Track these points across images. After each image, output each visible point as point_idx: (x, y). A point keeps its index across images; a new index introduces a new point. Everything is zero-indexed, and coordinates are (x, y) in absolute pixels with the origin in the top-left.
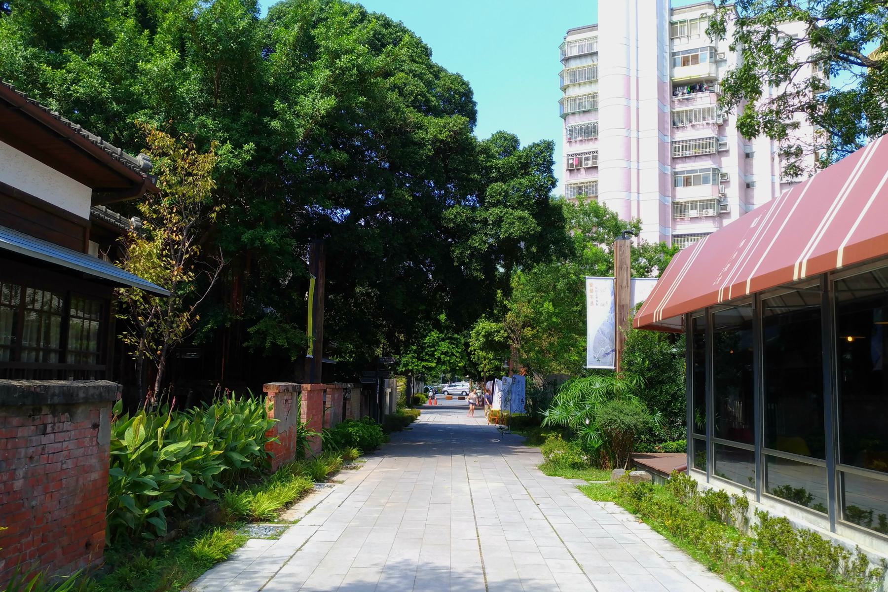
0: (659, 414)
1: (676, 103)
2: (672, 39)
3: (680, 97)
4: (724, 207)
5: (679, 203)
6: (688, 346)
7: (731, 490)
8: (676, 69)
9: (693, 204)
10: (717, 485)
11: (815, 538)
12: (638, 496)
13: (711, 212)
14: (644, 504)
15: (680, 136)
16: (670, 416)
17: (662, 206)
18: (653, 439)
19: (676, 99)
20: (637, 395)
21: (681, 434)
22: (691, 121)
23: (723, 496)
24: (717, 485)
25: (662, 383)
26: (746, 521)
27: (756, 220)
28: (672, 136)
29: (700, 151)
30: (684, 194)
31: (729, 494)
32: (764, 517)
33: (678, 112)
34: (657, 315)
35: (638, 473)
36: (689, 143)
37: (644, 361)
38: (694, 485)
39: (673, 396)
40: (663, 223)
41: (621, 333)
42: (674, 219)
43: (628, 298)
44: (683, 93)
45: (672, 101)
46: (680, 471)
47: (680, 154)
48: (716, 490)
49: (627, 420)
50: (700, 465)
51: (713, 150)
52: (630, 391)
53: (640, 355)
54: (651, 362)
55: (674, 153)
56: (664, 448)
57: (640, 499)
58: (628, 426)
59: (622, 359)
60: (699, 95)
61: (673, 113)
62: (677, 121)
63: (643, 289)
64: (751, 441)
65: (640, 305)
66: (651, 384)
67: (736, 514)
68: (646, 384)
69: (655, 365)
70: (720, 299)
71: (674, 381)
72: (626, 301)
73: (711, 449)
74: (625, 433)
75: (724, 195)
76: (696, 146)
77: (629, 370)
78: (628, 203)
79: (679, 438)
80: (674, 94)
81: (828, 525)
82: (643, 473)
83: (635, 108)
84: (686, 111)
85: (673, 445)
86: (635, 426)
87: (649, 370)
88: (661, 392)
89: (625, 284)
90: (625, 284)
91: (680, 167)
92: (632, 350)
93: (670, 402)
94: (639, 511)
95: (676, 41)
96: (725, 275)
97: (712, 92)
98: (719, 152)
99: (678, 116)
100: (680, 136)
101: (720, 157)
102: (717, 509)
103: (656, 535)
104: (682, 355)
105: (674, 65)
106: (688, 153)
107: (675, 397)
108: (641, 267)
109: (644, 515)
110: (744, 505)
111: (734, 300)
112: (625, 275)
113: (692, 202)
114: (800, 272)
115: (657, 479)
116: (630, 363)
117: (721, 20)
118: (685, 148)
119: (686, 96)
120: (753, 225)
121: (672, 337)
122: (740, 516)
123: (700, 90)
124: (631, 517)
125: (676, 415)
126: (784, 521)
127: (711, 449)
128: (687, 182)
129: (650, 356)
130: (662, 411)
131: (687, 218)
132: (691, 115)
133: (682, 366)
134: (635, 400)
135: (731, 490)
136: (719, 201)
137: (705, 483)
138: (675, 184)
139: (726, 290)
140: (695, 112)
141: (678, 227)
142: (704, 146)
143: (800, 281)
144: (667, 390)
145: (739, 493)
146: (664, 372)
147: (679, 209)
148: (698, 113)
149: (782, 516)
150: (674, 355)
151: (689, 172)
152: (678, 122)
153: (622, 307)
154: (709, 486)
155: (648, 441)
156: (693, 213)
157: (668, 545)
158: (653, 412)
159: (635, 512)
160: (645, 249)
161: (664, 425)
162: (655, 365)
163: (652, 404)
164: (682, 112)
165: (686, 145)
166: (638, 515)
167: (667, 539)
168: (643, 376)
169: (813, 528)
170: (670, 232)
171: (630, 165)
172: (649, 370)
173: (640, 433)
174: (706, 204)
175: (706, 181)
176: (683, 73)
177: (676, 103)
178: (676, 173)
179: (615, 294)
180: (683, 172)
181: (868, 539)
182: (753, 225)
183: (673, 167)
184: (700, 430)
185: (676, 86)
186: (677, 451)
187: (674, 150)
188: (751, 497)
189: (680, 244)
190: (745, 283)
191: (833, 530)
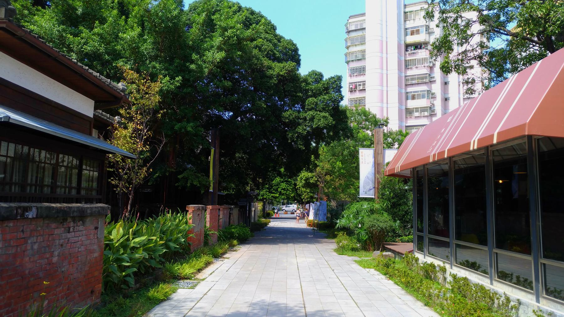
0: (398, 222)
2: (405, 21)
3: (410, 52)
4: (433, 111)
5: (409, 109)
6: (414, 186)
7: (437, 262)
9: (417, 109)
10: (429, 260)
12: (387, 266)
13: (426, 114)
15: (409, 73)
16: (404, 227)
17: (400, 110)
18: (395, 235)
19: (407, 53)
21: (410, 232)
22: (415, 65)
23: (432, 266)
25: (400, 205)
26: (445, 279)
27: (450, 118)
29: (420, 81)
30: (412, 104)
31: (436, 265)
32: (454, 277)
33: (408, 60)
35: (387, 253)
38: (417, 260)
39: (406, 212)
40: (400, 119)
41: (378, 179)
42: (406, 118)
45: (405, 54)
46: (409, 252)
47: (410, 82)
48: (429, 262)
49: (381, 225)
50: (421, 249)
51: (427, 80)
54: (394, 194)
56: (401, 240)
57: (388, 267)
58: (382, 228)
60: (419, 51)
62: (407, 65)
63: (390, 155)
64: (447, 236)
65: (388, 164)
66: (394, 205)
67: (440, 275)
68: (391, 206)
70: (431, 160)
71: (406, 204)
72: (380, 161)
73: (426, 241)
75: (433, 104)
76: (418, 78)
77: (382, 198)
80: (406, 50)
82: (390, 253)
87: (393, 198)
88: (400, 210)
89: (380, 152)
90: (380, 152)
91: (410, 89)
92: (384, 187)
93: (404, 215)
94: (387, 274)
95: (408, 22)
96: (434, 147)
97: (427, 49)
98: (430, 82)
100: (409, 73)
102: (429, 273)
103: (397, 287)
104: (410, 190)
105: (406, 35)
106: (413, 82)
107: (407, 213)
109: (390, 276)
110: (444, 270)
111: (438, 161)
112: (380, 147)
113: (416, 108)
114: (474, 146)
115: (397, 256)
116: (383, 195)
118: (412, 79)
120: (449, 121)
121: (406, 180)
122: (442, 276)
123: (420, 48)
124: (383, 277)
126: (465, 279)
127: (426, 241)
128: (413, 98)
129: (393, 190)
130: (400, 220)
133: (411, 196)
134: (385, 214)
135: (437, 262)
136: (430, 108)
137: (423, 259)
138: (407, 99)
139: (434, 155)
142: (422, 78)
143: (474, 150)
145: (441, 264)
146: (401, 199)
147: (409, 112)
148: (419, 60)
150: (406, 190)
153: (378, 164)
154: (425, 260)
155: (393, 236)
156: (417, 114)
157: (403, 292)
158: (395, 221)
159: (385, 274)
161: (401, 228)
162: (396, 196)
164: (411, 60)
165: (413, 77)
166: (387, 276)
168: (390, 201)
169: (481, 282)
172: (393, 198)
173: (388, 232)
174: (423, 109)
175: (423, 97)
176: (411, 39)
178: (407, 93)
180: (411, 92)
181: (523, 294)
182: (449, 121)
183: (406, 90)
185: (407, 46)
186: (408, 242)
187: (406, 80)
188: (447, 266)
189: (410, 131)
191: (492, 284)
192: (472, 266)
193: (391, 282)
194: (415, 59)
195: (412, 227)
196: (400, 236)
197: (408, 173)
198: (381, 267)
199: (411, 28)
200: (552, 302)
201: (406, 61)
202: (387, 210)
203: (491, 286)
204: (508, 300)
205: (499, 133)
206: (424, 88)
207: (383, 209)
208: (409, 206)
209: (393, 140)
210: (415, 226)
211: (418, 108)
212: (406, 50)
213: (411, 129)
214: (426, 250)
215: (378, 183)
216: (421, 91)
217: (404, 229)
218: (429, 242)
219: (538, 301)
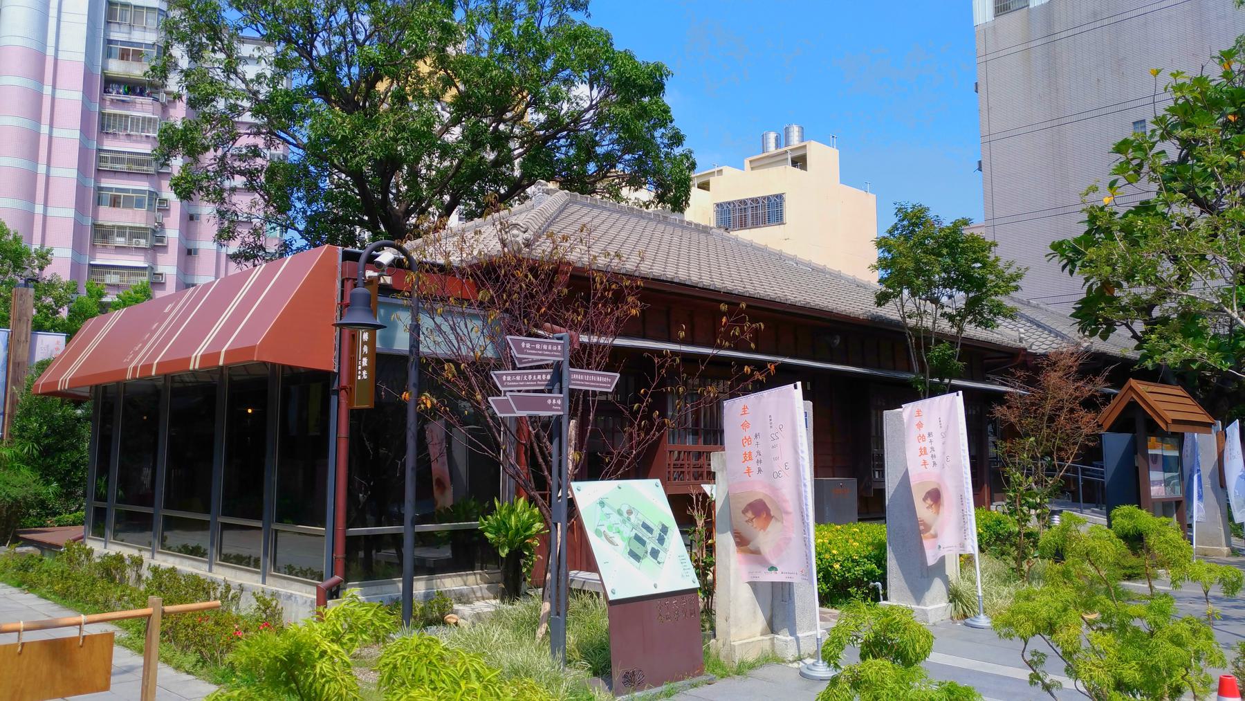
0: (55, 484)
1: (108, 103)
2: (108, 23)
3: (114, 96)
4: (161, 239)
5: (102, 226)
6: (95, 408)
7: (127, 552)
8: (111, 61)
9: (121, 231)
10: (113, 549)
11: (195, 577)
12: (25, 568)
13: (143, 243)
14: (32, 574)
15: (110, 145)
16: (67, 495)
17: (78, 227)
18: (46, 511)
19: (108, 97)
20: (28, 464)
21: (81, 505)
22: (126, 129)
23: (119, 558)
24: (113, 549)
25: (62, 450)
26: (139, 577)
27: (170, 306)
28: (100, 142)
29: (135, 168)
30: (109, 216)
31: (125, 556)
32: (155, 570)
33: (109, 115)
34: (64, 380)
35: (24, 549)
36: (121, 156)
37: (41, 426)
38: (90, 553)
39: (74, 464)
40: (77, 247)
41: (13, 395)
42: (93, 246)
43: (26, 354)
44: (118, 93)
45: (102, 100)
46: (75, 541)
47: (108, 166)
48: (113, 553)
49: (14, 492)
50: (99, 531)
51: (152, 170)
52: (17, 457)
53: (36, 421)
54: (49, 427)
55: (96, 164)
56: (58, 521)
57: (26, 571)
58: (15, 499)
59: (12, 423)
60: (139, 99)
61: (102, 115)
62: (106, 125)
63: (49, 344)
64: (151, 505)
65: (44, 365)
66: (47, 452)
67: (130, 573)
68: (40, 452)
69: (54, 431)
70: (129, 376)
71: (77, 448)
72: (22, 353)
73: (111, 519)
74: (10, 507)
75: (162, 225)
76: (130, 161)
77: (21, 436)
78: (30, 216)
79: (76, 511)
80: (106, 90)
81: (206, 567)
82: (30, 548)
83: (49, 98)
84: (121, 116)
85: (68, 517)
86: (24, 498)
87: (46, 436)
88: (60, 460)
89: (23, 338)
90: (23, 338)
91: (107, 183)
92: (28, 413)
93: (70, 471)
94: (24, 583)
95: (114, 27)
96: (136, 354)
97: (157, 100)
98: (159, 173)
99: (109, 119)
100: (110, 145)
101: (160, 179)
102: (111, 570)
103: (43, 601)
104: (87, 419)
105: (108, 54)
106: (118, 166)
107: (75, 466)
108: (46, 307)
109: (31, 586)
110: (138, 563)
111: (140, 379)
112: (26, 328)
113: (119, 227)
114: (195, 365)
115: (47, 553)
116: (23, 429)
117: (109, 304)
118: (114, 160)
119: (122, 97)
120: (166, 310)
121: (78, 402)
122: (134, 574)
123: (141, 94)
124: (15, 590)
125: (75, 484)
126: (173, 570)
127: (111, 519)
128: (115, 202)
129: (48, 420)
130: (58, 481)
131: (111, 245)
132: (126, 121)
133: (87, 431)
134: (25, 471)
135: (127, 552)
136: (154, 231)
137: (100, 548)
138: (99, 202)
139: (135, 368)
140: (132, 119)
141: (98, 255)
142: (140, 163)
143: (194, 371)
144: (67, 458)
145: (136, 553)
146: (64, 438)
147: (102, 234)
148: (136, 120)
149: (171, 566)
150: (78, 419)
151: (118, 190)
152: (109, 126)
153: (17, 365)
154: (106, 551)
155: (39, 516)
156: (120, 241)
157: (56, 607)
158: (48, 483)
159: (19, 586)
160: (51, 285)
161: (61, 496)
162: (53, 431)
163: (46, 474)
164: (115, 115)
165: (117, 157)
166: (25, 587)
167: (56, 603)
168: (39, 443)
169: (195, 571)
170: (87, 260)
171: (36, 168)
172: (46, 436)
173: (30, 506)
174: (136, 233)
175: (139, 204)
176: (116, 67)
177: (108, 103)
178: (101, 189)
179: (8, 347)
180: (110, 189)
181: (248, 575)
182: (166, 310)
183: (97, 180)
184: (100, 498)
185: (109, 82)
186: (74, 524)
187: (101, 159)
188: (146, 556)
189: (100, 277)
190: (152, 365)
191: (210, 570)
192: (194, 552)
193: (30, 596)
194: (127, 117)
195: (85, 495)
196: (55, 514)
197: (85, 391)
198: (10, 572)
199: (123, 43)
200: (285, 582)
201: (102, 115)
202: (29, 461)
203: (210, 575)
204: (228, 588)
205: (227, 352)
206: (144, 185)
207: (22, 461)
208: (81, 453)
209: (56, 301)
210: (92, 489)
211: (124, 227)
212: (106, 90)
213: (103, 274)
214: (108, 533)
215: (12, 404)
216: (135, 191)
217: (68, 500)
218: (118, 521)
219: (264, 582)
